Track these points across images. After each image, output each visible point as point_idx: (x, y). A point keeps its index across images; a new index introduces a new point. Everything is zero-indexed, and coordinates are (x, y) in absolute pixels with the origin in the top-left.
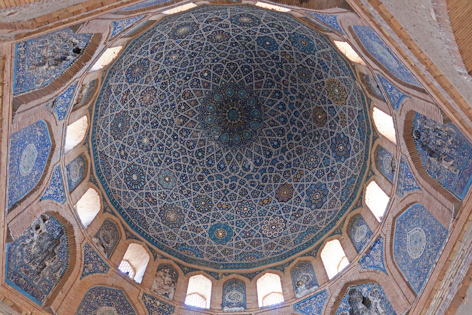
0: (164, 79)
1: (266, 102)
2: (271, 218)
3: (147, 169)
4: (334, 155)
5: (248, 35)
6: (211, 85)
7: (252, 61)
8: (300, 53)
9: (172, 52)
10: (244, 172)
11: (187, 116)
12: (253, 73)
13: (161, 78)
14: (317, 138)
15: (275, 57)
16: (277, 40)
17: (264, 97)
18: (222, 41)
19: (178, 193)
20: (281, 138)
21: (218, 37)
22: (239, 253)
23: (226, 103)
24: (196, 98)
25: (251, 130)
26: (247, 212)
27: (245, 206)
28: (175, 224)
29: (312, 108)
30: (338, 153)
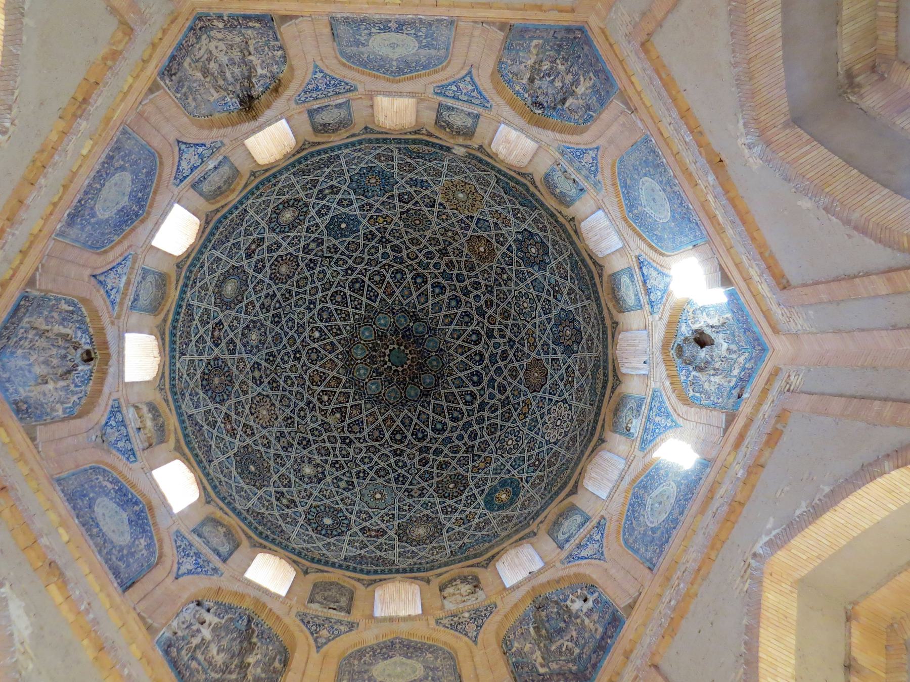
0: (267, 376)
1: (417, 303)
2: (546, 418)
3: (339, 502)
4: (536, 267)
5: (313, 236)
6: (336, 342)
7: (353, 269)
8: (385, 199)
9: (246, 332)
10: (470, 408)
11: (341, 405)
12: (369, 283)
13: (261, 377)
14: (505, 276)
15: (370, 236)
16: (346, 210)
17: (410, 299)
18: (294, 273)
19: (407, 500)
20: (474, 324)
21: (284, 269)
22: (542, 490)
23: (375, 351)
24: (332, 374)
25: (434, 354)
26: (515, 443)
27: (506, 439)
28: (433, 535)
29: (466, 251)
30: (537, 260)
